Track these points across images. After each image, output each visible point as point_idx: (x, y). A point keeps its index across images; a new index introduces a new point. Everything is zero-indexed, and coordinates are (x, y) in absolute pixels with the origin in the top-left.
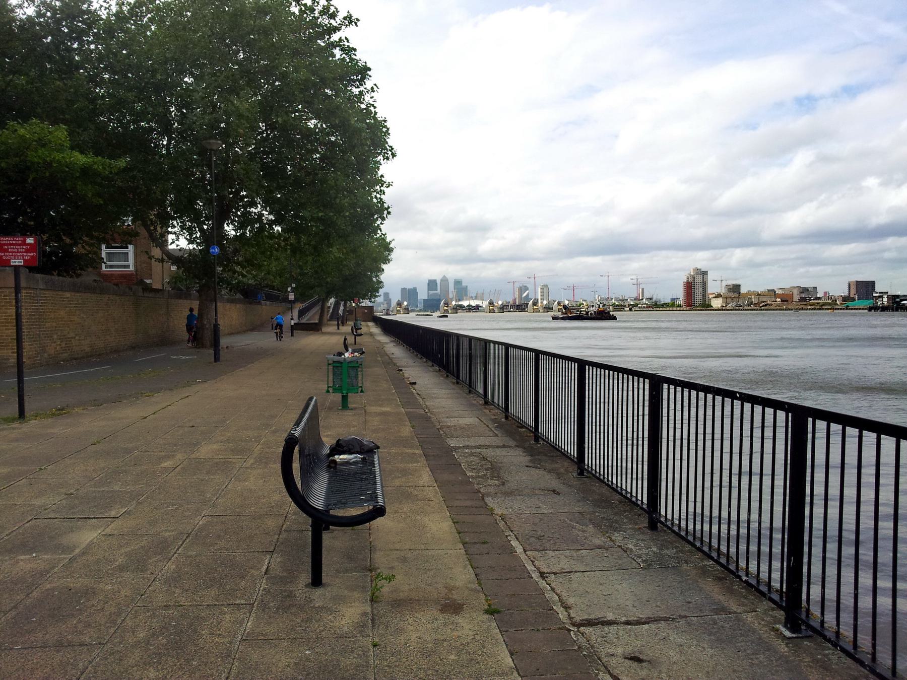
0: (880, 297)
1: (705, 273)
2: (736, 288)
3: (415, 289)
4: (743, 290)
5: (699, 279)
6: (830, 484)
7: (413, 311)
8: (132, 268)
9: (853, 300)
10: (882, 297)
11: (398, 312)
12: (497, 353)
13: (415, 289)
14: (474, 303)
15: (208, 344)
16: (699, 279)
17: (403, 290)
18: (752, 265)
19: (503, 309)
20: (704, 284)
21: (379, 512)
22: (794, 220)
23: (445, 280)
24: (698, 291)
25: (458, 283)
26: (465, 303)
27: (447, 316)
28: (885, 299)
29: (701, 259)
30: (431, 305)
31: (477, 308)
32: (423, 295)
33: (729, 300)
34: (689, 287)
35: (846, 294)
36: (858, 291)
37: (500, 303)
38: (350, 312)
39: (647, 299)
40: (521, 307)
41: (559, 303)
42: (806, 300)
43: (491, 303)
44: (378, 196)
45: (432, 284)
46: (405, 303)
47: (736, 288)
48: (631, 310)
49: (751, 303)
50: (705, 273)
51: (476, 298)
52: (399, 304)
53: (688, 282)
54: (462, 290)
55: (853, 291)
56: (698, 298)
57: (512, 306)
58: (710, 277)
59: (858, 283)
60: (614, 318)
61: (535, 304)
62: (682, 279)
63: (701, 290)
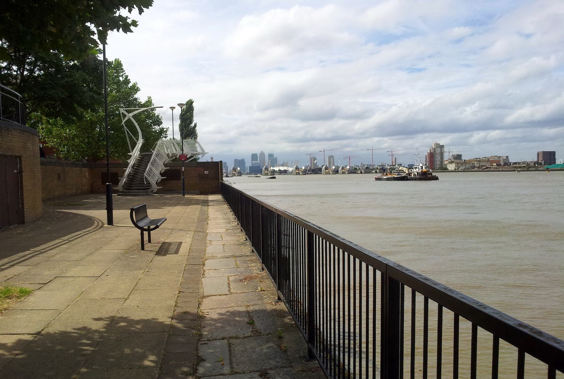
1: (442, 147)
2: (459, 157)
3: (243, 160)
4: (463, 158)
5: (438, 151)
6: (491, 351)
7: (243, 174)
8: (259, 161)
9: (541, 164)
11: (234, 175)
14: (282, 168)
15: (148, 220)
16: (438, 151)
17: (236, 161)
19: (305, 172)
20: (442, 154)
22: (525, 112)
23: (262, 154)
24: (438, 158)
25: (271, 156)
26: (276, 169)
27: (275, 178)
30: (256, 170)
31: (285, 172)
32: (248, 164)
33: (460, 165)
34: (432, 156)
35: (536, 160)
36: (544, 158)
37: (303, 168)
39: (398, 165)
40: (316, 171)
41: (343, 168)
42: (502, 165)
43: (297, 168)
44: (112, 149)
45: (254, 157)
46: (239, 169)
47: (459, 157)
49: (475, 167)
51: (283, 165)
52: (234, 169)
53: (431, 153)
54: (273, 160)
55: (541, 158)
56: (438, 163)
57: (309, 170)
58: (446, 149)
59: (544, 153)
60: (436, 178)
61: (326, 168)
62: (426, 151)
63: (439, 158)
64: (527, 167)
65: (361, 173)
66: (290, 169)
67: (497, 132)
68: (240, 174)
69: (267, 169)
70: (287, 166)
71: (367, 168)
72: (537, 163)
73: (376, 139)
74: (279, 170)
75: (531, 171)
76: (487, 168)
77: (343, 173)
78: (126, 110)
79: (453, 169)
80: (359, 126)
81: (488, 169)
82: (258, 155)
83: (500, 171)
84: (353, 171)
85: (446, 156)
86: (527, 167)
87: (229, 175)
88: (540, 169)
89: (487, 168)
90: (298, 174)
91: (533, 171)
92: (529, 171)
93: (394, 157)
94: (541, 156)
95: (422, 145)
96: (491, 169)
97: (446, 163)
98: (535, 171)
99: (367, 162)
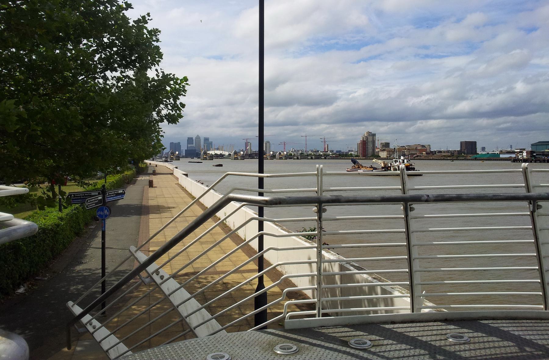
0: (520, 152)
1: (374, 135)
3: (179, 143)
4: (392, 147)
8: (194, 145)
10: (522, 152)
12: (358, 289)
13: (179, 143)
14: (218, 152)
16: (370, 139)
18: (394, 132)
19: (243, 158)
20: (374, 142)
21: (185, 96)
23: (198, 138)
24: (370, 146)
25: (206, 139)
28: (525, 154)
29: (371, 127)
32: (184, 148)
34: (364, 144)
38: (82, 182)
39: (330, 151)
41: (280, 153)
43: (236, 153)
45: (190, 140)
46: (177, 153)
47: (387, 145)
48: (325, 158)
50: (374, 135)
51: (218, 149)
52: (173, 153)
53: (363, 141)
54: (208, 143)
55: (464, 148)
56: (370, 150)
62: (359, 139)
63: (371, 146)
64: (452, 156)
65: (298, 158)
66: (227, 153)
67: (362, 127)
68: (178, 158)
69: (205, 153)
70: (222, 150)
71: (301, 154)
72: (459, 152)
73: (324, 126)
74: (216, 154)
75: (460, 160)
76: (417, 156)
77: (281, 158)
78: (350, 270)
79: (385, 156)
80: (315, 112)
81: (419, 158)
82: (194, 139)
83: (431, 159)
84: (289, 157)
85: (378, 144)
86: (452, 156)
87: (168, 160)
88: (469, 158)
89: (417, 156)
90: (236, 159)
91: (462, 160)
92: (458, 160)
93: (327, 143)
94: (464, 145)
95: (358, 132)
96: (422, 158)
97: (377, 150)
98: (464, 160)
99: (301, 148)
